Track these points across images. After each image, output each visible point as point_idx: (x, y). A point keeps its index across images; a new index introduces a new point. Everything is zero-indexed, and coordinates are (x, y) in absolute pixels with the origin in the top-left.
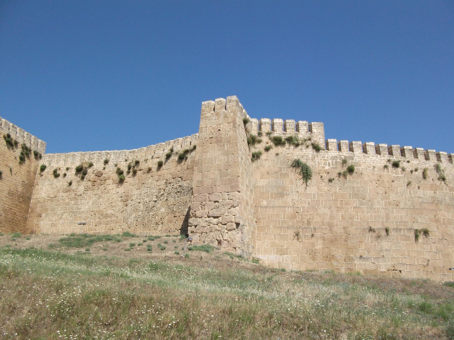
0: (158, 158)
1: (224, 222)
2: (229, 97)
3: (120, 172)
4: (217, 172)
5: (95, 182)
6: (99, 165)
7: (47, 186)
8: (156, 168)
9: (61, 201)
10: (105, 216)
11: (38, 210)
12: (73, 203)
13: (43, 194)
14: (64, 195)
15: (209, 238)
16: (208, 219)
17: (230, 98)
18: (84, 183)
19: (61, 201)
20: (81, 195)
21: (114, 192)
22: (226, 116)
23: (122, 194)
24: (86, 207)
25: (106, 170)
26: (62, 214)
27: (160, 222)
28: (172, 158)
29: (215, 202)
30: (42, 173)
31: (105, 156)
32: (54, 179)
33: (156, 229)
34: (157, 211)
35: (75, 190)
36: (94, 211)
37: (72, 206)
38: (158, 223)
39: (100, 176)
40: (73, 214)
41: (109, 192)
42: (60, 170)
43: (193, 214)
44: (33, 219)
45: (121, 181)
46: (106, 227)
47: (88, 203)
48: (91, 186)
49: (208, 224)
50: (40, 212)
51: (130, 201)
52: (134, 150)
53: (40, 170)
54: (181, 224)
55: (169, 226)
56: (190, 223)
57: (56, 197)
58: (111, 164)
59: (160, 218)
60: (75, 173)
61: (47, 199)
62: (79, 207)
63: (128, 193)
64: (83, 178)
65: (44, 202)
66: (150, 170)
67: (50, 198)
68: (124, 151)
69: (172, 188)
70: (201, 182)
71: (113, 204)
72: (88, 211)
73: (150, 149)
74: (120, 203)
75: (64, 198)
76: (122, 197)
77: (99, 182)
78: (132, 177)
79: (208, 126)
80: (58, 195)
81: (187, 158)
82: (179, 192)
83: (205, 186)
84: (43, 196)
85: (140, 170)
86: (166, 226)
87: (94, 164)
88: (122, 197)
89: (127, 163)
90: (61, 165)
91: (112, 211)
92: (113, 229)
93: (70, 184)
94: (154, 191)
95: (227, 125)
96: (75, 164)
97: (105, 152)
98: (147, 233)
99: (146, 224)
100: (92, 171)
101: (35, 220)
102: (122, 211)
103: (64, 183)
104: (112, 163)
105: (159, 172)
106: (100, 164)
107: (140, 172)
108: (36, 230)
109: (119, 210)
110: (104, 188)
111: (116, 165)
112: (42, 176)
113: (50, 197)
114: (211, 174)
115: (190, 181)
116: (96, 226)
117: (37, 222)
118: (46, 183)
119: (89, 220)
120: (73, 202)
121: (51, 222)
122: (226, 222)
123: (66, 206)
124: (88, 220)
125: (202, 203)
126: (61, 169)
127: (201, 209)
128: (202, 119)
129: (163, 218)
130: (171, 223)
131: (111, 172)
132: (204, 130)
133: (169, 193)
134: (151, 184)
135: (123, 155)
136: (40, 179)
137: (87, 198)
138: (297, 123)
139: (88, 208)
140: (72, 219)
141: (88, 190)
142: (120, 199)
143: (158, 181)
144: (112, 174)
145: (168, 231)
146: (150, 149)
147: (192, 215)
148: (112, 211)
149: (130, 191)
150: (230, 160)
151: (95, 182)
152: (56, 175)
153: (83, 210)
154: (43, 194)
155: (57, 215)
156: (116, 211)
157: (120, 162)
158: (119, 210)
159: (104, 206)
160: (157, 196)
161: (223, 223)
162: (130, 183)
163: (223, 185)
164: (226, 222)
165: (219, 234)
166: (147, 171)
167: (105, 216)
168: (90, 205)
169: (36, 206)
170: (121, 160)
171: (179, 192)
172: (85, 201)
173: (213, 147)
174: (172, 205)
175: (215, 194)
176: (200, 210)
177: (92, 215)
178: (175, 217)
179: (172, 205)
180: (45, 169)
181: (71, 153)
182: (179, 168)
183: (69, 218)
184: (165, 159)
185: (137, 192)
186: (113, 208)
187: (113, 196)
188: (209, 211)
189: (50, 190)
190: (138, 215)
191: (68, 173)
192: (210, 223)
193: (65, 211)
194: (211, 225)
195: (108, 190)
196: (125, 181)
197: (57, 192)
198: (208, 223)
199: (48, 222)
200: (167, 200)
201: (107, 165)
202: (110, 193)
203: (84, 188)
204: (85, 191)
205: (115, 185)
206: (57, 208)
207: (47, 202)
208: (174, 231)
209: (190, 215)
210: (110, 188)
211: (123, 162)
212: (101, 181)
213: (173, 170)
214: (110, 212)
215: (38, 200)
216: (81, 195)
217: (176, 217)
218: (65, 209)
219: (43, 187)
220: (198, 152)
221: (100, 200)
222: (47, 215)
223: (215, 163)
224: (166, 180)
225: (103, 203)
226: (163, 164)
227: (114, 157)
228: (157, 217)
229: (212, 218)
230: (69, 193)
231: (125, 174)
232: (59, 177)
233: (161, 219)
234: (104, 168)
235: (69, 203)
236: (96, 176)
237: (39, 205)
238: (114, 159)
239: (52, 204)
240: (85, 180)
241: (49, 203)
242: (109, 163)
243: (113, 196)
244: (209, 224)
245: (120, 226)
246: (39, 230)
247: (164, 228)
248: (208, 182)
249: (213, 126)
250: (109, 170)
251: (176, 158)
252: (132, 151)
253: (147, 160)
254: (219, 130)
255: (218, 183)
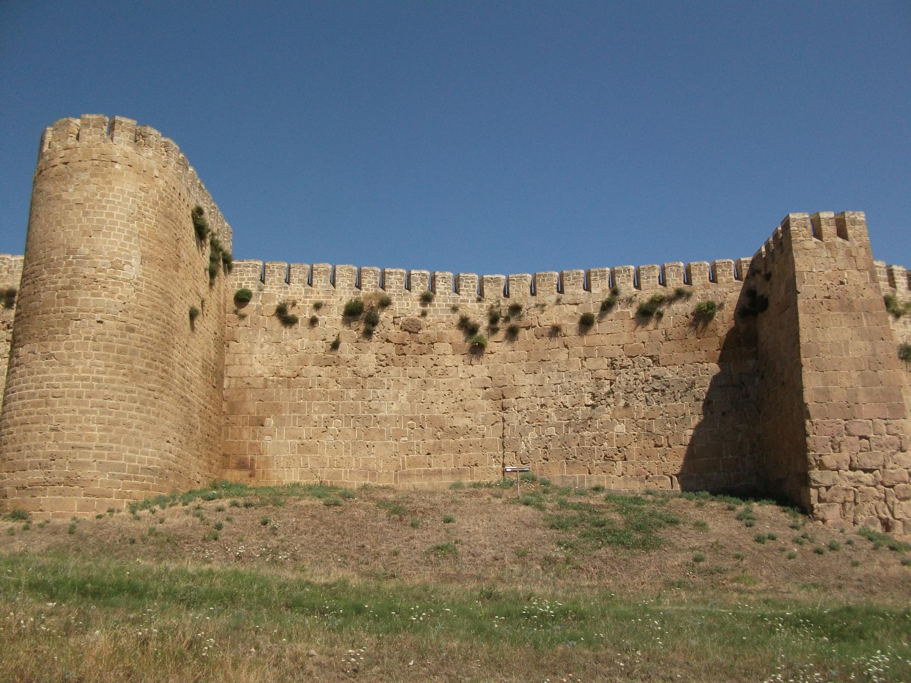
0: (576, 304)
1: (887, 480)
2: (851, 212)
3: (467, 327)
4: (855, 374)
5: (404, 345)
6: (408, 303)
7: (266, 346)
8: (574, 327)
9: (316, 388)
10: (451, 432)
11: (252, 407)
12: (353, 396)
13: (257, 365)
14: (322, 373)
15: (865, 515)
16: (851, 473)
17: (853, 214)
18: (375, 344)
19: (316, 388)
20: (372, 376)
21: (461, 375)
22: (849, 254)
23: (485, 380)
24: (394, 407)
25: (428, 318)
26: (326, 421)
27: (616, 455)
28: (619, 310)
29: (861, 437)
30: (243, 311)
31: (419, 282)
32: (283, 328)
33: (608, 472)
34: (606, 430)
35: (351, 363)
36: (417, 418)
37: (352, 401)
38: (612, 457)
39: (416, 330)
40: (357, 423)
41: (447, 372)
42: (297, 307)
43: (816, 461)
44: (241, 431)
45: (477, 349)
46: (456, 458)
47: (396, 396)
48: (394, 354)
49: (853, 484)
50: (258, 413)
51: (513, 400)
52: (496, 276)
53: (233, 302)
54: (681, 461)
55: (645, 466)
56: (814, 481)
57: (298, 376)
58: (439, 305)
59: (615, 447)
60: (343, 320)
61: (273, 381)
62: (374, 404)
63: (504, 379)
64: (368, 334)
65: (266, 386)
66: (555, 331)
67: (281, 377)
68: (469, 276)
69: (635, 379)
70: (825, 393)
71: (468, 404)
72: (400, 418)
73: (548, 280)
74: (486, 402)
75: (324, 379)
76: (485, 388)
77: (414, 346)
78: (505, 342)
79: (814, 270)
80: (303, 371)
81: (660, 315)
82: (656, 390)
83: (834, 401)
84: (259, 372)
85: (528, 328)
86: (635, 464)
87: (394, 300)
88: (485, 388)
89: (482, 306)
90: (295, 293)
91: (467, 421)
92: (476, 465)
93: (335, 346)
94: (583, 382)
95: (856, 273)
96: (339, 296)
97: (418, 272)
98: (582, 480)
99: (575, 457)
100: (391, 317)
101: (245, 434)
102: (492, 423)
103: (317, 342)
104: (444, 301)
105: (585, 338)
106: (410, 302)
107: (526, 331)
108: (252, 460)
109: (486, 420)
110: (433, 363)
111: (455, 309)
112: (243, 317)
113: (282, 374)
114: (844, 378)
115: (681, 369)
116: (429, 454)
117: (254, 438)
118: (259, 336)
119: (406, 439)
120: (352, 393)
121: (298, 441)
122: (894, 482)
123: (334, 402)
124: (403, 439)
125: (833, 437)
126: (298, 304)
127: (834, 452)
128: (796, 252)
129: (625, 447)
130: (648, 460)
131: (444, 325)
132: (807, 278)
133: (629, 391)
134: (567, 364)
135: (469, 287)
136: (238, 326)
137: (390, 386)
138: (112, 121)
139: (398, 409)
140: (360, 437)
141: (387, 365)
142: (481, 392)
143: (585, 358)
144: (446, 329)
145: (644, 476)
146: (548, 280)
147: (814, 463)
148: (467, 421)
149: (509, 377)
150: (878, 351)
151: (404, 345)
152: (285, 317)
153: (386, 413)
154: (257, 365)
155: (312, 423)
156: (477, 421)
157: (462, 301)
158: (486, 420)
159: (443, 408)
160: (593, 394)
161: (888, 484)
162: (504, 356)
163: (873, 404)
164: (894, 482)
165: (883, 507)
166: (547, 331)
167: (449, 433)
168: (403, 402)
169: (242, 396)
170: (466, 298)
171: (656, 390)
172: (386, 392)
173: (837, 318)
174: (644, 418)
175: (860, 422)
176: (832, 453)
177: (412, 429)
178: (656, 446)
179: (644, 418)
180: (248, 301)
181: (322, 265)
182: (642, 334)
183: (350, 432)
184: (599, 310)
185: (529, 379)
186: (468, 414)
187: (462, 385)
188: (853, 456)
189: (277, 358)
190: (547, 434)
191: (322, 317)
192: (859, 481)
193: (334, 414)
194: (862, 487)
195: (444, 367)
196: (487, 350)
197: (298, 365)
198: (855, 482)
199: (289, 441)
200: (626, 406)
201: (428, 307)
202: (451, 375)
203: (376, 358)
204: (381, 365)
205: (460, 358)
206: (309, 405)
207: (276, 387)
208: (661, 478)
209: (811, 464)
210: (447, 364)
211: (472, 301)
212: (421, 343)
213: (625, 338)
214: (461, 422)
215: (247, 380)
216: (371, 376)
217: (661, 446)
218: (334, 408)
219: (252, 347)
220: (805, 326)
221: (429, 392)
222: (281, 422)
223: (848, 354)
224: (611, 358)
225: (437, 400)
226: (596, 320)
227: (445, 288)
228: (606, 444)
229: (861, 473)
230: (336, 369)
231: (482, 331)
232: (296, 325)
233: (618, 447)
234: (424, 314)
235: (341, 394)
236: (405, 330)
237: (250, 395)
238: (446, 294)
239: (291, 393)
240: (374, 337)
241: (283, 390)
242: (435, 302)
243: (462, 385)
244: (857, 485)
245: (494, 457)
246: (263, 458)
247: (632, 470)
248: (838, 395)
249: (826, 272)
250: (436, 318)
251: (632, 311)
252: (492, 279)
253: (544, 305)
254: (842, 283)
255: (862, 398)
